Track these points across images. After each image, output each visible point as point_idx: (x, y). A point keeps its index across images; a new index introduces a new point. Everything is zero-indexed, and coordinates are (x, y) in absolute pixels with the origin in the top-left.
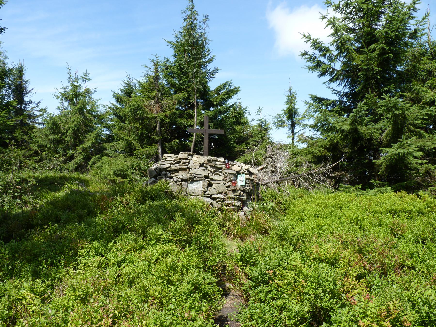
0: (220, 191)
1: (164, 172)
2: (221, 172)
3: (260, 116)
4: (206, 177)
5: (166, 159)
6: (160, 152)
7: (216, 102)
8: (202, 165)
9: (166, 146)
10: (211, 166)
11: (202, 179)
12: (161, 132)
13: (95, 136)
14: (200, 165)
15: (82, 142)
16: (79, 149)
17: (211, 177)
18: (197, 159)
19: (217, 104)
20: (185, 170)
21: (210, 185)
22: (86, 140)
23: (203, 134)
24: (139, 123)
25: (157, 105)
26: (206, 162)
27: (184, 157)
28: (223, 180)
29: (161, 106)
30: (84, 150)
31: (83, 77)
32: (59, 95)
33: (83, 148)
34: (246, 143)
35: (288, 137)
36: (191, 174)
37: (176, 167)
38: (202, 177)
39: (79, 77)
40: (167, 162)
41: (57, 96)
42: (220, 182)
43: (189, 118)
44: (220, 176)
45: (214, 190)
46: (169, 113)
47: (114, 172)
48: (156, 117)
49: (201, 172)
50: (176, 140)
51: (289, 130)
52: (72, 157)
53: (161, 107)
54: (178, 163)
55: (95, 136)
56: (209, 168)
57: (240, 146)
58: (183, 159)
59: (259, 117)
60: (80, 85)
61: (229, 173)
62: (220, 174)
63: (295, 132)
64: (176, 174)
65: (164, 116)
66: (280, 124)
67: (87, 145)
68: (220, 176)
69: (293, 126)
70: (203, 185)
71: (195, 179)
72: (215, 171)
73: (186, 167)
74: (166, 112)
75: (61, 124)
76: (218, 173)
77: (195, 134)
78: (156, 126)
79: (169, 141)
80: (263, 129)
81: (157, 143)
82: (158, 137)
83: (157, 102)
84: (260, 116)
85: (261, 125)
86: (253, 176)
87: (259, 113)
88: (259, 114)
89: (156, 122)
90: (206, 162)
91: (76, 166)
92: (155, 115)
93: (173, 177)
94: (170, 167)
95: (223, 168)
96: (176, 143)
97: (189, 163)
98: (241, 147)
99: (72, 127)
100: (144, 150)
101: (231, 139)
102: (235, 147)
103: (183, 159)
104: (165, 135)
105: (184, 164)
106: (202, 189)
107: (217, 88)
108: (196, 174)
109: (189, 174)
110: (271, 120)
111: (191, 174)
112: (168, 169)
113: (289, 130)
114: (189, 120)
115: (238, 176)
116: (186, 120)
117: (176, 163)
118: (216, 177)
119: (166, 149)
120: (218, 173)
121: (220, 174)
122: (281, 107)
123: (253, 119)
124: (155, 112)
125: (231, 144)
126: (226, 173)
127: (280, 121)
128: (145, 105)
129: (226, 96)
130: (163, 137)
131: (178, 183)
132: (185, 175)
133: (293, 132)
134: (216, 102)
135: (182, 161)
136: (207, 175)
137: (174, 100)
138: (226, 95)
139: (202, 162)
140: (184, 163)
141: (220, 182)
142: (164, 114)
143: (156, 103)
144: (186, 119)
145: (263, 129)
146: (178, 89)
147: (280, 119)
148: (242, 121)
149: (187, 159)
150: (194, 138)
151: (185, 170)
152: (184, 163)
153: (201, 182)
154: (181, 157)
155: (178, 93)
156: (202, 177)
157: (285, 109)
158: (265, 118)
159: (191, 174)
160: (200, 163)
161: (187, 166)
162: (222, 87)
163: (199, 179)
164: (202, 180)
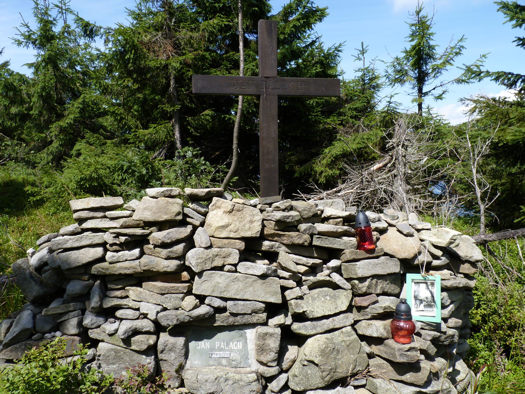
0: (341, 373)
1: (74, 287)
2: (338, 270)
3: (362, 62)
4: (272, 309)
5: (81, 221)
6: (177, 135)
7: (284, 34)
8: (252, 249)
9: (189, 124)
10: (295, 248)
11: (255, 319)
12: (178, 95)
13: (81, 106)
14: (242, 245)
15: (60, 116)
16: (54, 129)
17: (296, 307)
18: (226, 219)
19: (285, 38)
20: (171, 277)
21: (290, 337)
22: (66, 113)
23: (258, 97)
24: (132, 78)
25: (168, 42)
26: (270, 230)
27: (164, 217)
28: (350, 309)
29: (176, 44)
30: (62, 130)
31: (57, 6)
32: (21, 39)
33: (61, 126)
34: (340, 114)
35: (413, 101)
36: (201, 299)
37: (127, 261)
38: (255, 312)
39: (51, 6)
40: (89, 238)
41: (19, 41)
42: (337, 322)
43: (231, 68)
44: (335, 286)
45: (311, 370)
46: (190, 56)
47: (78, 182)
48: (166, 66)
49: (247, 285)
50: (207, 112)
51: (413, 88)
52: (46, 143)
53: (177, 46)
54: (138, 242)
55: (81, 106)
56: (286, 258)
57: (328, 120)
58: (161, 225)
59: (360, 64)
60: (54, 20)
61: (374, 277)
62: (336, 278)
63: (424, 91)
64: (133, 292)
65: (181, 63)
66: (399, 77)
67: (66, 121)
68: (335, 286)
69: (421, 79)
70: (261, 349)
71: (221, 320)
72: (313, 270)
73: (172, 265)
74: (184, 54)
75: (23, 87)
76: (321, 276)
77: (240, 97)
78: (169, 85)
79: (194, 113)
80: (369, 84)
81: (170, 119)
82: (173, 105)
83: (166, 37)
84: (362, 62)
85: (363, 80)
86: (466, 268)
87: (361, 56)
88: (360, 59)
89: (168, 79)
90: (270, 230)
91: (51, 157)
92: (163, 63)
93: (119, 307)
94: (102, 259)
95: (348, 254)
96: (208, 118)
97: (189, 242)
98: (331, 122)
99: (38, 93)
100: (146, 132)
101: (313, 107)
102: (320, 123)
103: (161, 225)
104: (187, 102)
105: (164, 252)
106: (255, 366)
107: (285, 8)
108: (225, 299)
109: (190, 301)
110: (382, 68)
111: (197, 296)
112: (95, 269)
113: (413, 88)
114: (232, 71)
115: (410, 277)
116: (225, 72)
117: (128, 245)
118: (317, 303)
119: (189, 130)
120: (321, 276)
121: (336, 278)
122: (402, 44)
123: (348, 70)
124: (164, 57)
125: (312, 117)
126: (362, 280)
127: (399, 71)
128: (141, 42)
129: (302, 21)
130: (183, 105)
131: (140, 342)
132: (170, 301)
133: (420, 90)
134: (284, 34)
135: (158, 236)
136: (277, 299)
137: (200, 32)
138: (303, 19)
139: (254, 231)
140: (164, 245)
141: (337, 322)
142: (181, 58)
143: (165, 38)
144: (227, 70)
145: (369, 84)
146: (210, 11)
147: (398, 67)
148: (330, 72)
149: (183, 223)
150: (240, 107)
151: (171, 277)
152: (164, 245)
153: (251, 334)
154: (149, 216)
155: (210, 19)
156: (255, 312)
157: (409, 48)
158: (372, 66)
159: (197, 296)
160: (243, 239)
161: (182, 257)
162: (294, 6)
163: (239, 320)
164: (253, 325)
